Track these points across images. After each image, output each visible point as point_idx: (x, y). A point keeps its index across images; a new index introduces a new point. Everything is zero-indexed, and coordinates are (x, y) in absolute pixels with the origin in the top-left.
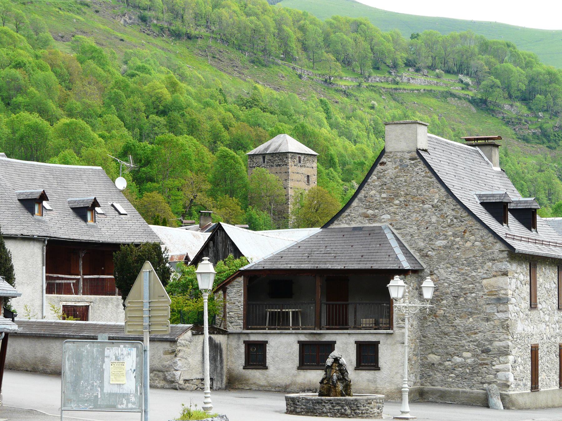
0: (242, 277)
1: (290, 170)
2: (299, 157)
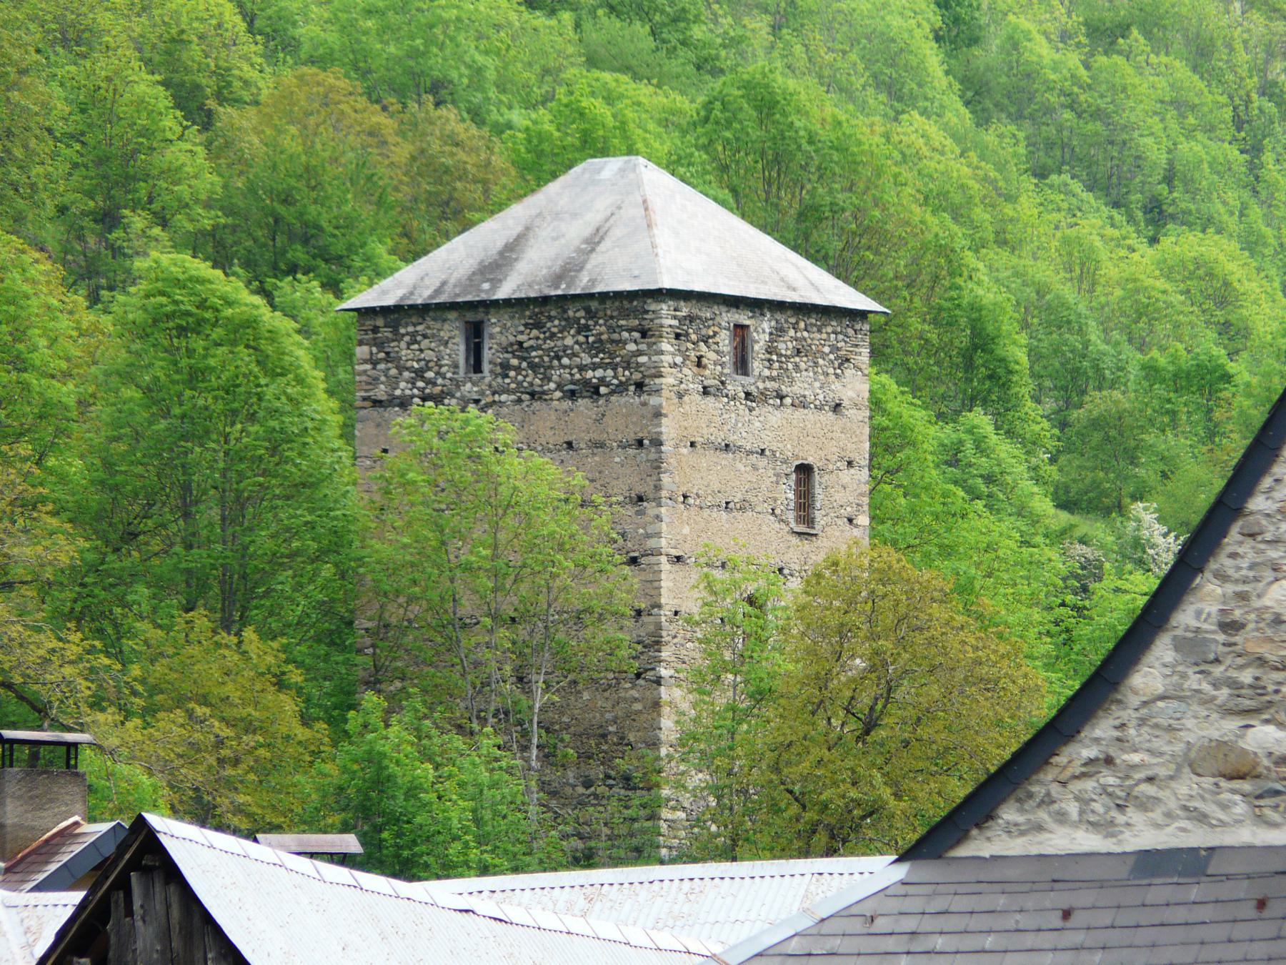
1: (668, 429)
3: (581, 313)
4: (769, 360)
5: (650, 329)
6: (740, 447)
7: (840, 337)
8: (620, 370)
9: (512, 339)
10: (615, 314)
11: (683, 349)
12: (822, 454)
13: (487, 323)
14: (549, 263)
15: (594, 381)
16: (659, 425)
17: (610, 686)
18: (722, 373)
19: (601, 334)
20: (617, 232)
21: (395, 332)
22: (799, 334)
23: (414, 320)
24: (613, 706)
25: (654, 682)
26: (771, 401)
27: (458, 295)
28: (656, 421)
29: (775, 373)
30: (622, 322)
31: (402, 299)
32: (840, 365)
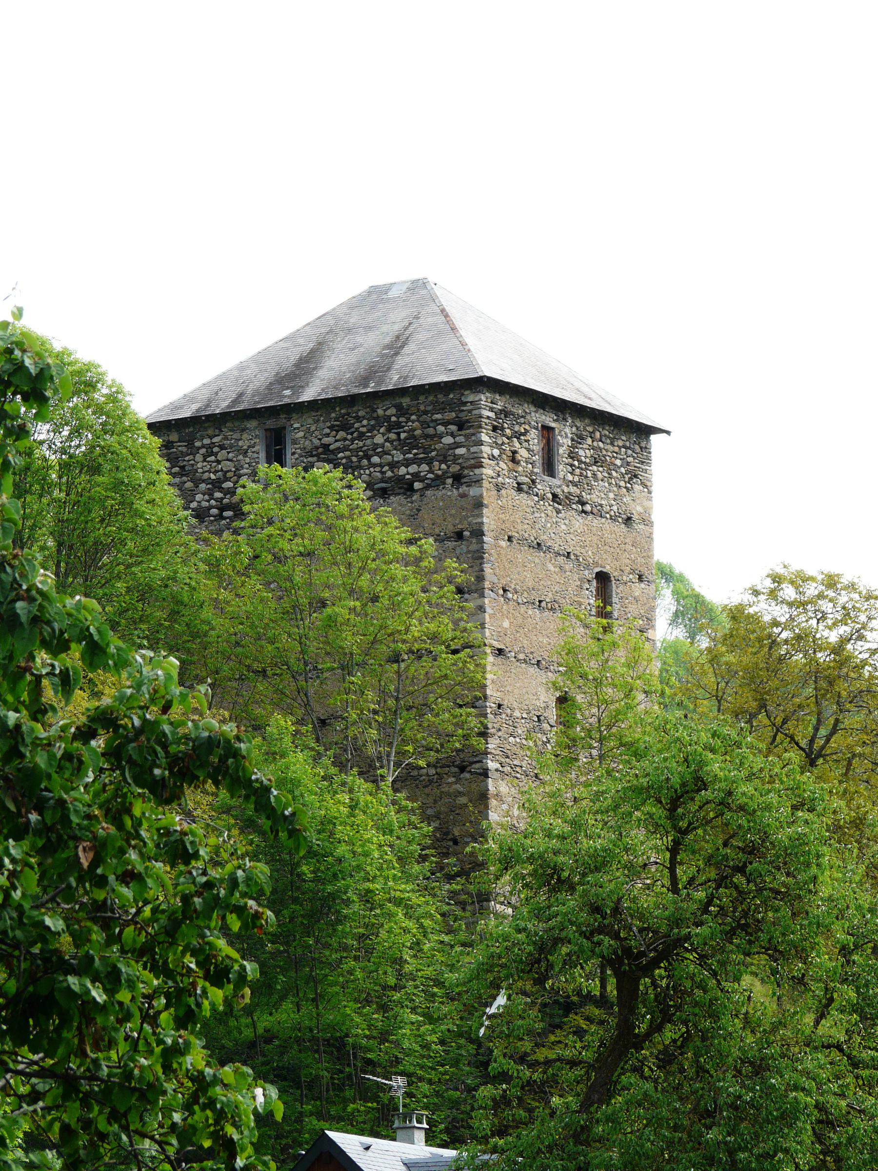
0: (11, 727)
1: (489, 519)
2: (547, 430)
3: (393, 411)
4: (572, 465)
5: (468, 421)
6: (549, 547)
7: (630, 452)
8: (436, 463)
9: (316, 442)
10: (429, 408)
11: (500, 442)
12: (618, 564)
13: (289, 429)
14: (352, 368)
15: (408, 477)
16: (481, 515)
17: (431, 782)
18: (532, 472)
19: (414, 430)
20: (420, 337)
21: (190, 444)
22: (595, 444)
23: (210, 432)
24: (435, 801)
25: (480, 774)
26: (574, 506)
27: (259, 402)
28: (476, 512)
29: (576, 479)
30: (439, 416)
31: (197, 411)
32: (631, 479)
